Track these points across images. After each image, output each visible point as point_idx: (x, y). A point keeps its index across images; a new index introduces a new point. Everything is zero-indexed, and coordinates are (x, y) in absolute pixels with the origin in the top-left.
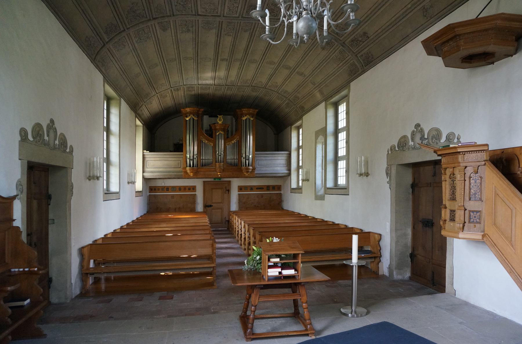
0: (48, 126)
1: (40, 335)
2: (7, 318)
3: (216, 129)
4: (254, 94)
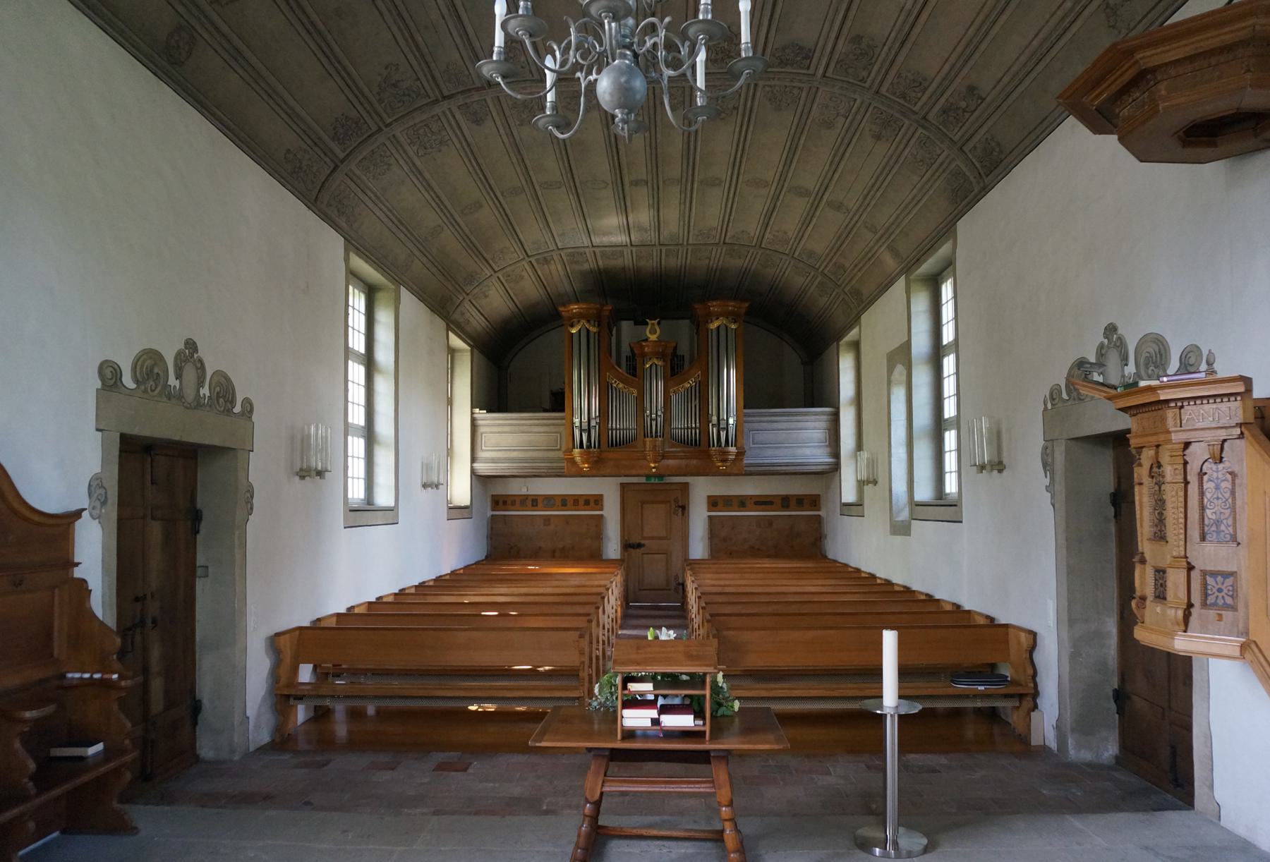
0: (179, 356)
1: (122, 827)
2: (26, 780)
3: (644, 355)
4: (737, 263)
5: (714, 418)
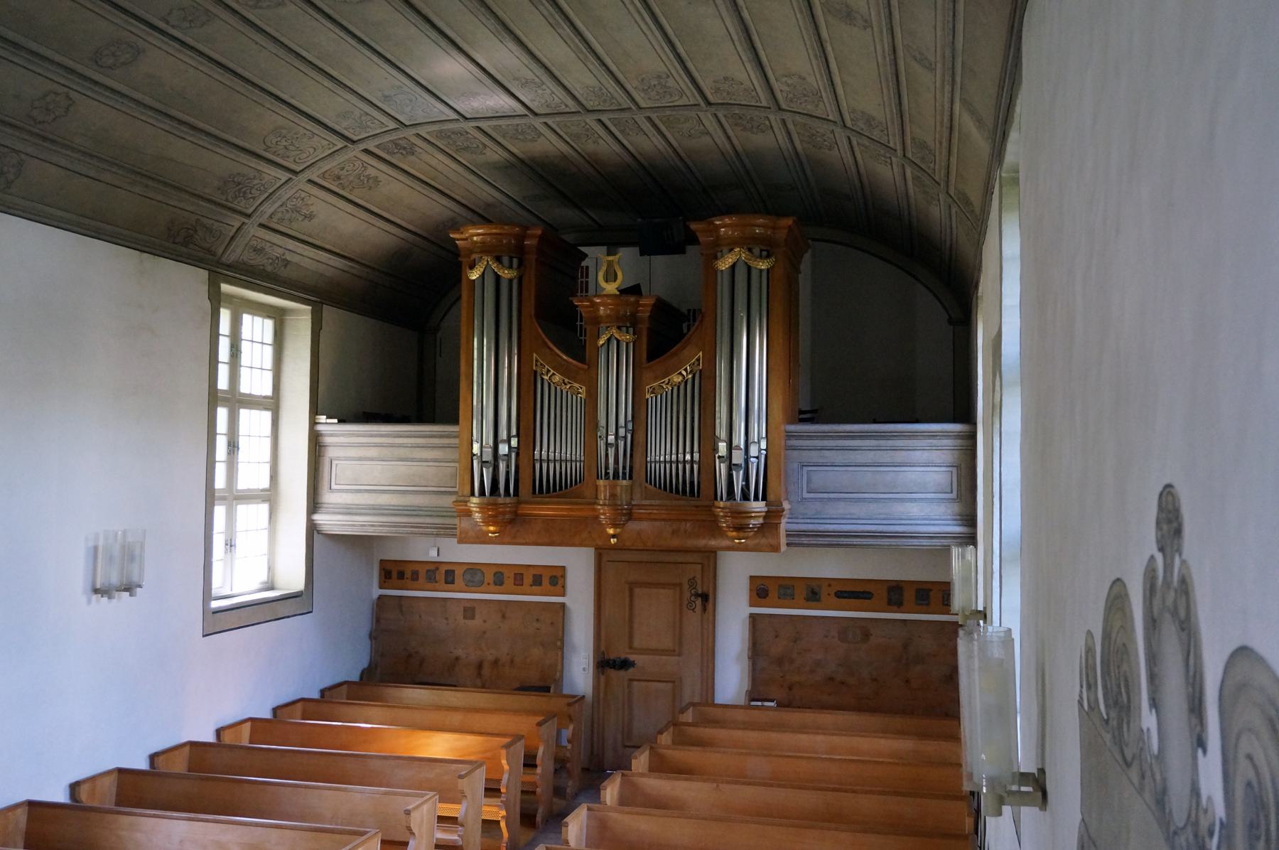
3: (596, 321)
5: (722, 447)
